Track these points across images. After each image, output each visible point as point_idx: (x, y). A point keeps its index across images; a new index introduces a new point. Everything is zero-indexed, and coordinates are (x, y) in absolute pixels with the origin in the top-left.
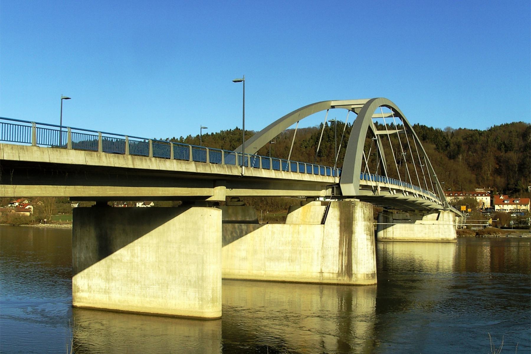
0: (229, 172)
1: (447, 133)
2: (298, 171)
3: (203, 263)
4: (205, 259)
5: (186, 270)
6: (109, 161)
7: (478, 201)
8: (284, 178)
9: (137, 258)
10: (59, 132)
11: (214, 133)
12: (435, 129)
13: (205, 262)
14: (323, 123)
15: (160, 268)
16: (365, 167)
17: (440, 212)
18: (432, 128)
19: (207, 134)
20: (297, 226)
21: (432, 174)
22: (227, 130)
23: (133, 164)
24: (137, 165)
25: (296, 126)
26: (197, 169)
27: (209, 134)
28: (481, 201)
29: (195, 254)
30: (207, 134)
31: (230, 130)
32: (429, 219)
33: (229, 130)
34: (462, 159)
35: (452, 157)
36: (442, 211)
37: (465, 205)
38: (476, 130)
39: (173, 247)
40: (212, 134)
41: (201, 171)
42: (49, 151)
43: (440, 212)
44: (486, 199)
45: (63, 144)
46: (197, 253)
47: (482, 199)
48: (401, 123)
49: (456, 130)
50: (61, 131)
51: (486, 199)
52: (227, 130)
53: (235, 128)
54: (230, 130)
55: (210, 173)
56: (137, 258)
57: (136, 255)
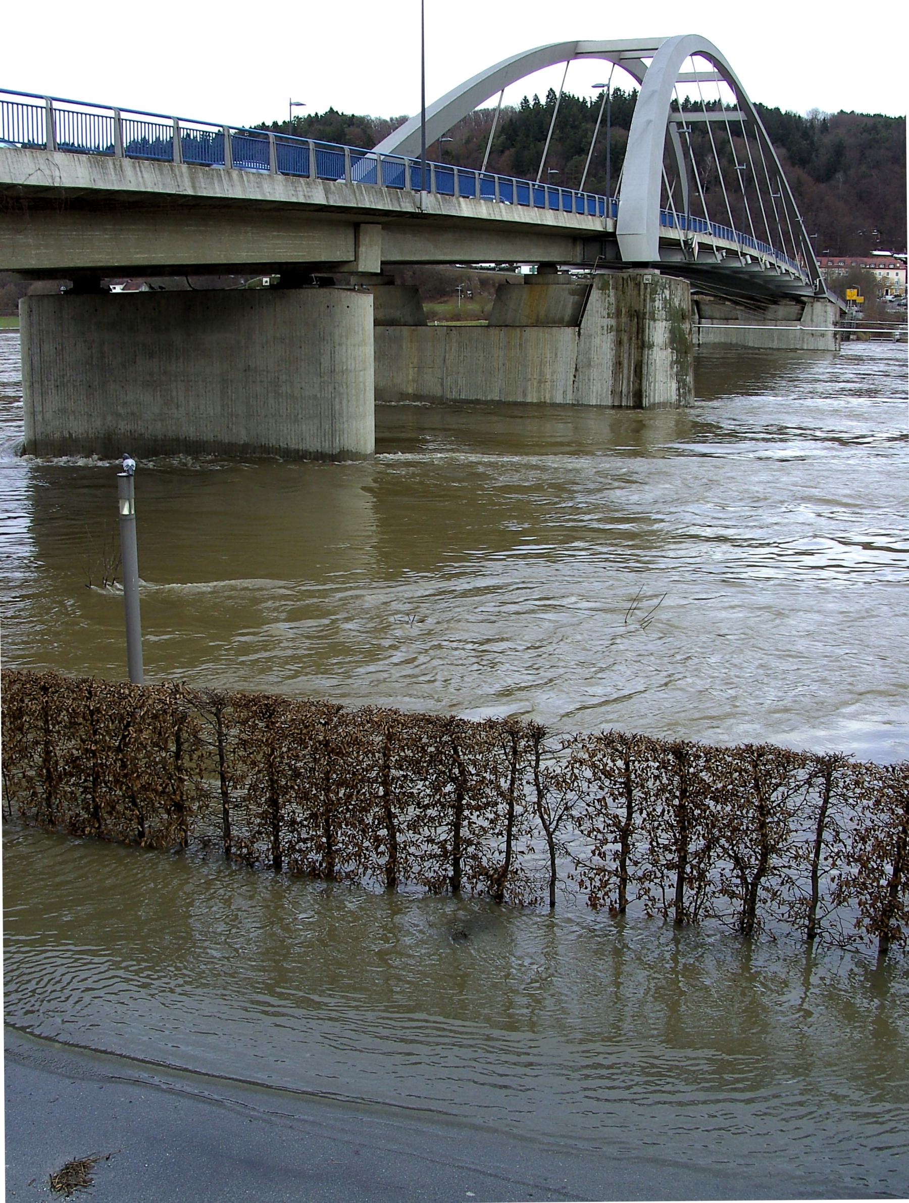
0: (393, 205)
1: (812, 121)
2: (532, 203)
3: (333, 417)
4: (337, 407)
5: (293, 433)
6: (140, 179)
7: (879, 277)
8: (505, 219)
9: (177, 408)
10: (44, 110)
11: (280, 123)
12: (783, 112)
13: (337, 415)
14: (528, 98)
15: (231, 430)
16: (674, 192)
17: (804, 303)
18: (777, 109)
19: (263, 124)
20: (518, 330)
21: (793, 215)
22: (309, 115)
23: (194, 187)
24: (200, 187)
25: (490, 103)
26: (327, 198)
27: (267, 124)
28: (885, 278)
29: (315, 397)
30: (263, 124)
31: (316, 114)
32: (779, 318)
33: (313, 115)
34: (845, 183)
35: (826, 175)
36: (811, 300)
37: (854, 288)
38: (880, 116)
39: (261, 382)
40: (275, 124)
41: (335, 201)
42: (8, 155)
43: (804, 303)
44: (897, 274)
45: (58, 141)
46: (319, 395)
47: (888, 274)
48: (730, 99)
49: (833, 116)
50: (51, 111)
51: (897, 274)
52: (309, 115)
53: (328, 110)
54: (316, 114)
55: (355, 205)
56: (177, 408)
57: (176, 401)
